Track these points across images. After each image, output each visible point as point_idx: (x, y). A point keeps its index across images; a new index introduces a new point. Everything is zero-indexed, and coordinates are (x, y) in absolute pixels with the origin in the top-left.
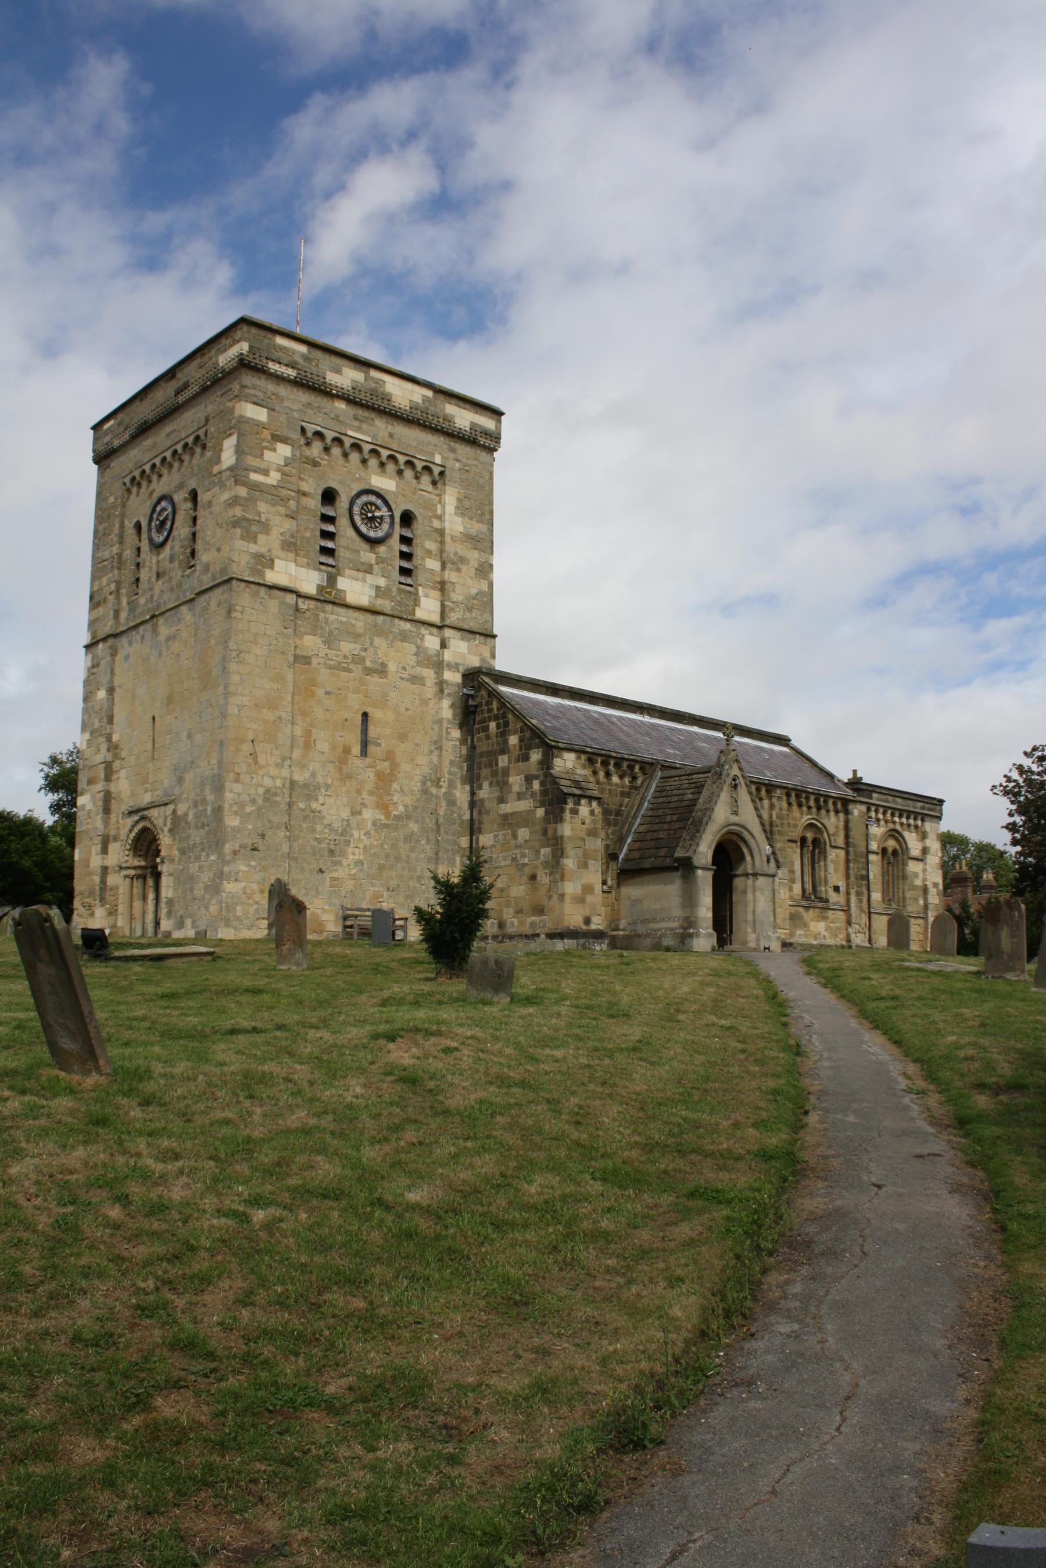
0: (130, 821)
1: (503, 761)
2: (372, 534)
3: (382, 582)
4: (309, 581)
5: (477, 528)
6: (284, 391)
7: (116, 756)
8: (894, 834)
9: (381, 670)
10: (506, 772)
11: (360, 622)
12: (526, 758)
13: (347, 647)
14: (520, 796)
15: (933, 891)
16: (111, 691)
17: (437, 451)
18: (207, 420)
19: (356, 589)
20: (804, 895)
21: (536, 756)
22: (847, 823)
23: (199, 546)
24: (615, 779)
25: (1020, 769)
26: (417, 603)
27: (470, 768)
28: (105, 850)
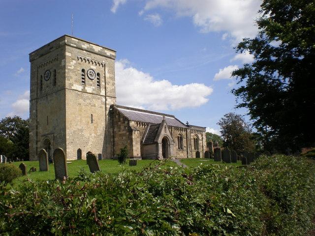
0: (43, 138)
1: (119, 123)
2: (92, 78)
3: (94, 88)
4: (80, 88)
5: (112, 75)
6: (74, 49)
7: (38, 124)
8: (197, 135)
9: (95, 106)
10: (120, 125)
11: (90, 96)
12: (124, 123)
13: (88, 101)
14: (123, 130)
15: (204, 147)
16: (37, 110)
17: (103, 60)
18: (58, 55)
19: (89, 89)
20: (179, 148)
21: (126, 122)
22: (186, 133)
23: (57, 81)
24: (141, 126)
25: (223, 119)
26: (101, 92)
27: (113, 125)
28: (37, 143)
